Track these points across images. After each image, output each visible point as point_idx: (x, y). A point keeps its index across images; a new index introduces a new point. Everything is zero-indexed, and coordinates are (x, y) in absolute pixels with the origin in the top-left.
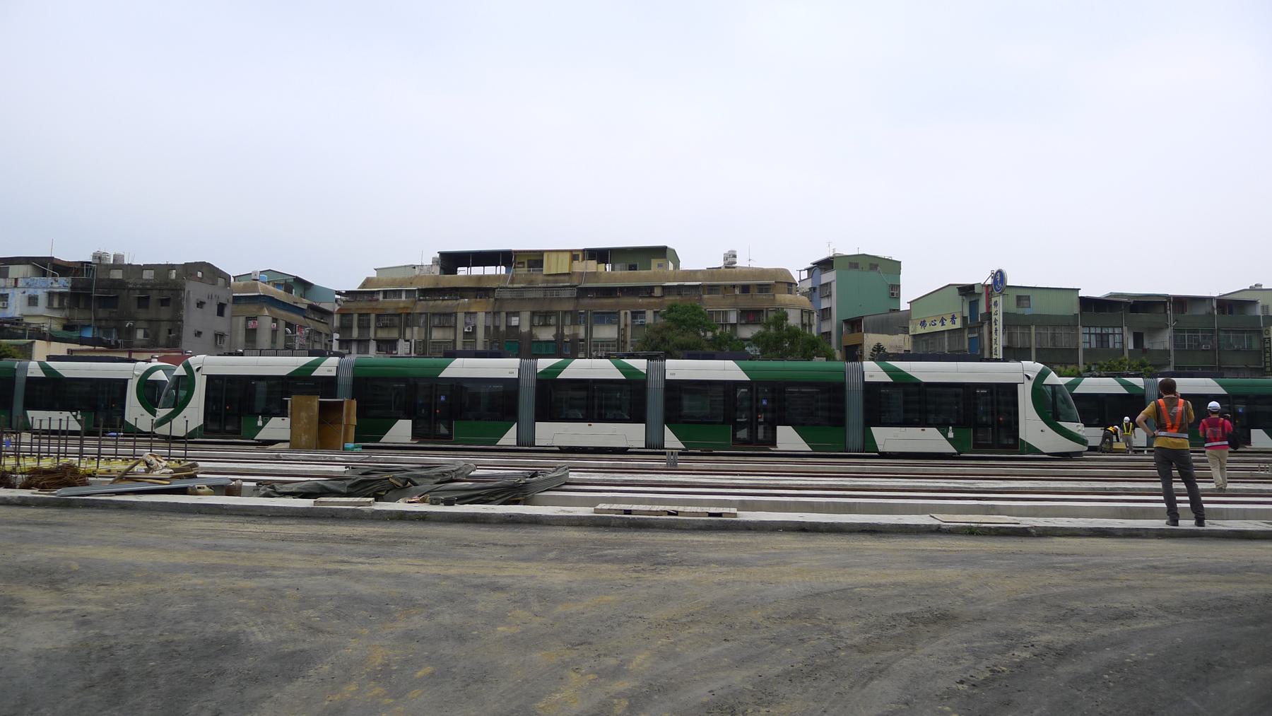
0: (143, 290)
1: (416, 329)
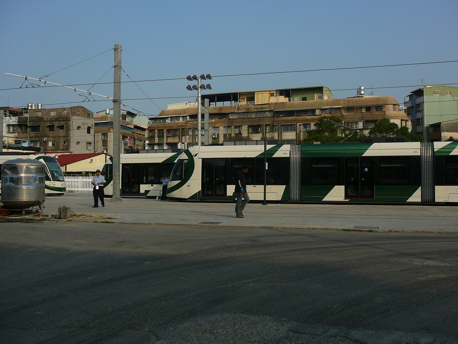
0: (51, 121)
1: (187, 137)
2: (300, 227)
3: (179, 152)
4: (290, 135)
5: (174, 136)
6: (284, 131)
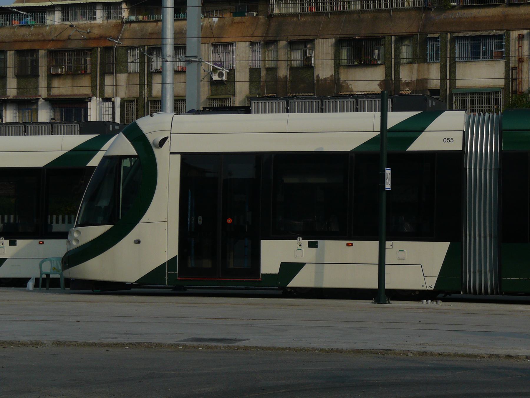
1: (122, 77)
2: (470, 351)
3: (104, 131)
4: (482, 74)
5: (75, 73)
6: (464, 57)
